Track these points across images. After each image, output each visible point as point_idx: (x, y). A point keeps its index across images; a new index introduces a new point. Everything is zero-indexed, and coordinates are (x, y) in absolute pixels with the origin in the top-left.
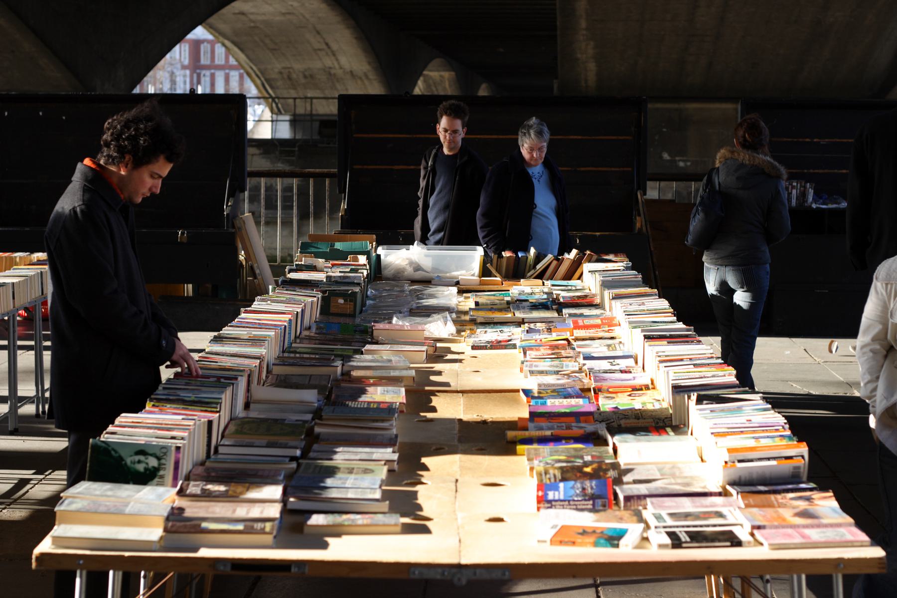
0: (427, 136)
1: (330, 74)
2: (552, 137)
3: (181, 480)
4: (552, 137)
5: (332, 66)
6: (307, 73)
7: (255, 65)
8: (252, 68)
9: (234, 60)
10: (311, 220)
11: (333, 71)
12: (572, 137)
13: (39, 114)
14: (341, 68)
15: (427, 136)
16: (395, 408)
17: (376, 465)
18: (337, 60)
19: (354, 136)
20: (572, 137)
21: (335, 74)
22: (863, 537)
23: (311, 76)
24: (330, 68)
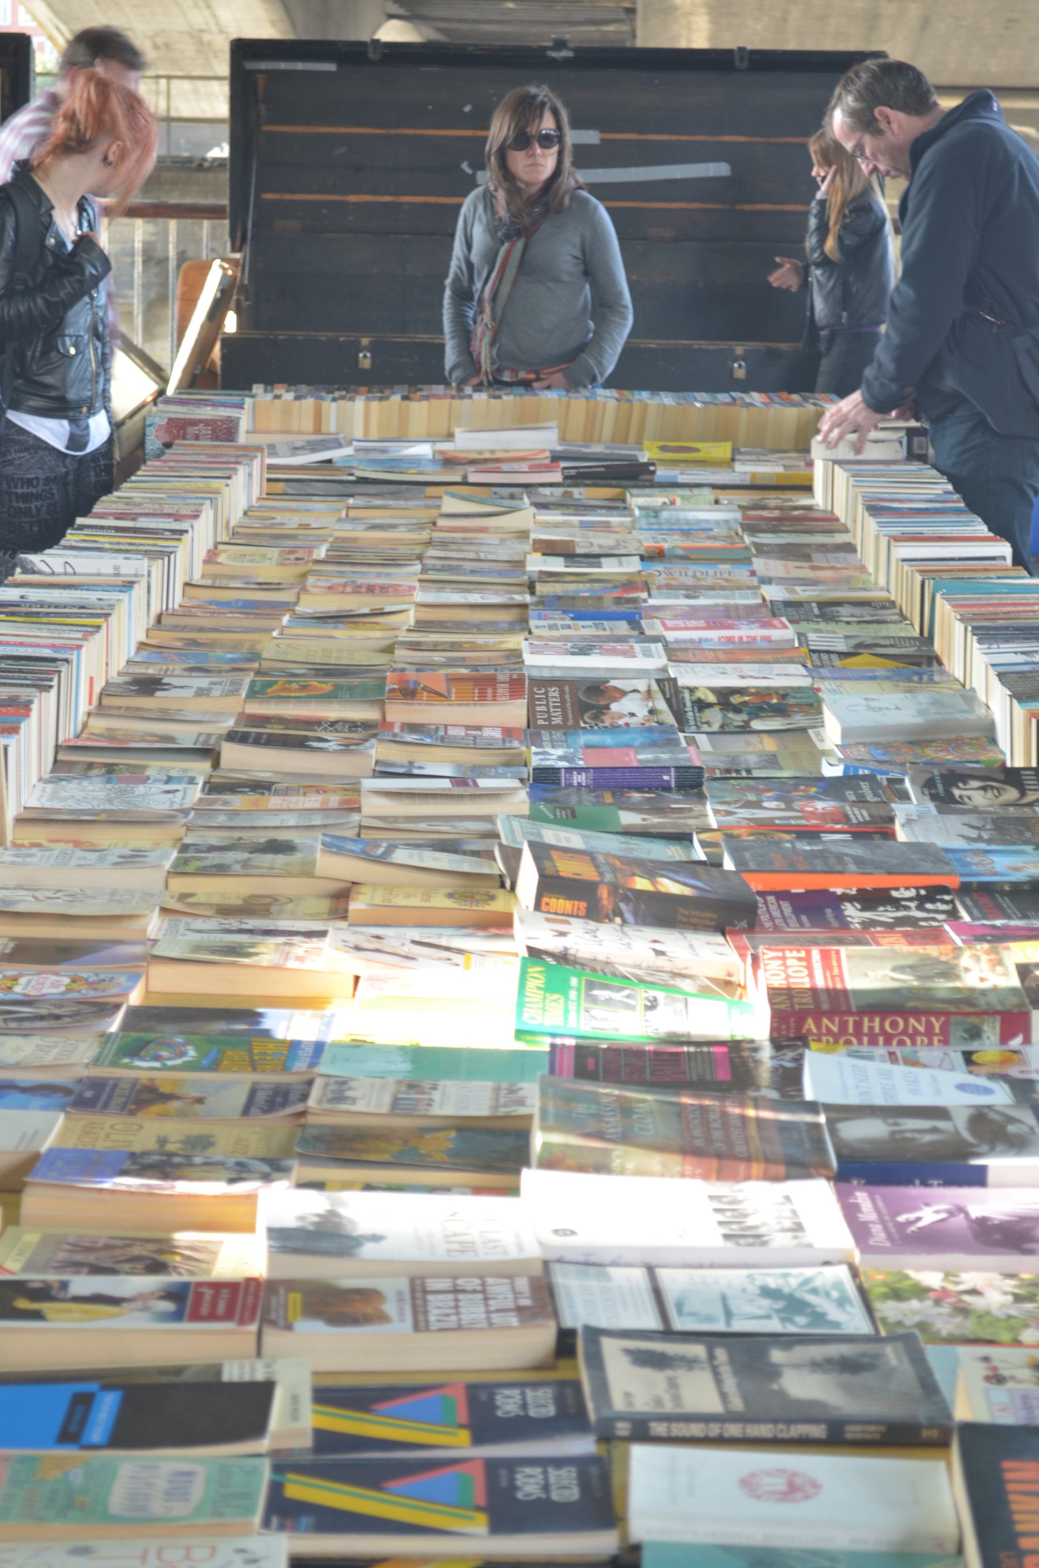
0: (419, 132)
1: (201, 42)
2: (480, 133)
3: (785, 467)
4: (480, 133)
5: (204, 27)
6: (159, 41)
7: (65, 23)
8: (58, 29)
9: (29, 17)
10: (138, 245)
11: (206, 38)
12: (727, 138)
13: (471, 112)
14: (221, 32)
15: (419, 132)
16: (879, 405)
17: (75, 557)
18: (214, 16)
19: (265, 128)
20: (727, 138)
21: (209, 43)
22: (982, 529)
23: (167, 45)
24: (202, 31)
